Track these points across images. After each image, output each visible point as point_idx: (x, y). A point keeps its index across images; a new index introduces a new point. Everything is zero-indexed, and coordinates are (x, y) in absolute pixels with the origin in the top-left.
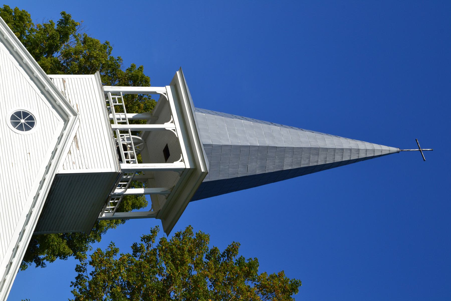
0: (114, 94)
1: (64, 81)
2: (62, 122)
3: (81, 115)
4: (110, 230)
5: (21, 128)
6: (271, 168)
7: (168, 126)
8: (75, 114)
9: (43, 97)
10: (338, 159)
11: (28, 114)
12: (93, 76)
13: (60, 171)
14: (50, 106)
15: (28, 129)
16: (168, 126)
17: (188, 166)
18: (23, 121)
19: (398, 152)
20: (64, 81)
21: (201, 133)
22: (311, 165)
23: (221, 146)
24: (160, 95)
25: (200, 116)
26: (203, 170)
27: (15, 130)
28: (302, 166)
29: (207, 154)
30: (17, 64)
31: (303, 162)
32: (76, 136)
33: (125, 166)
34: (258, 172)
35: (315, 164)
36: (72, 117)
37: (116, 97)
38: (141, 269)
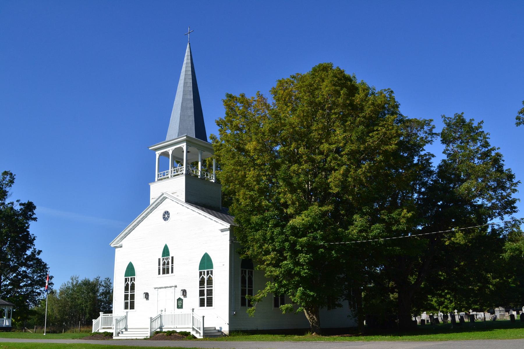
0: (158, 177)
1: (153, 199)
2: (167, 199)
3: (164, 191)
4: (493, 143)
5: (169, 217)
6: (192, 105)
7: (170, 153)
8: (163, 194)
9: (158, 208)
10: (190, 73)
11: (164, 214)
12: (151, 186)
13: (184, 200)
14: (161, 204)
15: (169, 214)
16: (170, 153)
17: (185, 144)
18: (166, 216)
19: (189, 44)
20: (153, 199)
21: (174, 138)
22: (192, 86)
23: (179, 128)
24: (162, 157)
25: (167, 138)
26: (185, 137)
27: (169, 219)
28: (192, 90)
29: (182, 135)
30: (146, 218)
31: (190, 90)
32: (172, 193)
33: (184, 172)
34: (193, 110)
35: (191, 84)
36: (164, 195)
37: (160, 175)
38: (395, 137)
